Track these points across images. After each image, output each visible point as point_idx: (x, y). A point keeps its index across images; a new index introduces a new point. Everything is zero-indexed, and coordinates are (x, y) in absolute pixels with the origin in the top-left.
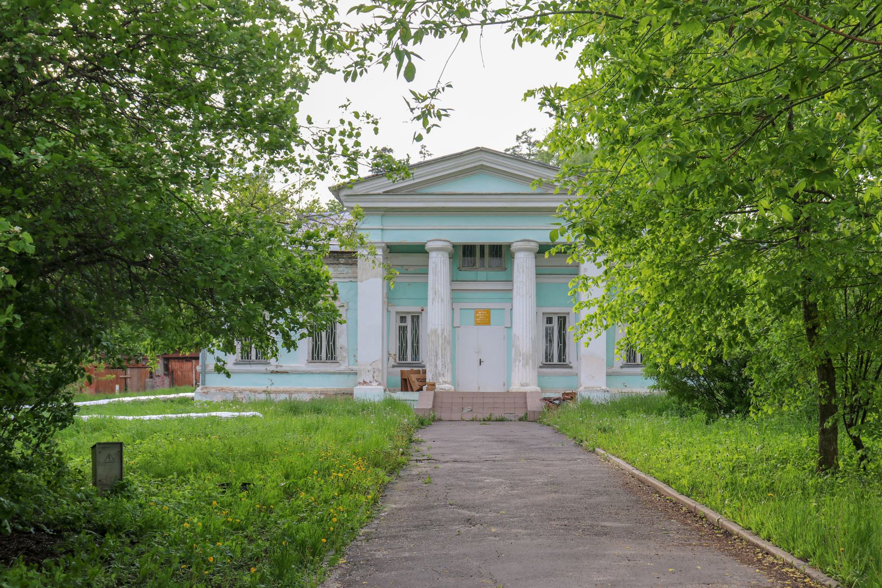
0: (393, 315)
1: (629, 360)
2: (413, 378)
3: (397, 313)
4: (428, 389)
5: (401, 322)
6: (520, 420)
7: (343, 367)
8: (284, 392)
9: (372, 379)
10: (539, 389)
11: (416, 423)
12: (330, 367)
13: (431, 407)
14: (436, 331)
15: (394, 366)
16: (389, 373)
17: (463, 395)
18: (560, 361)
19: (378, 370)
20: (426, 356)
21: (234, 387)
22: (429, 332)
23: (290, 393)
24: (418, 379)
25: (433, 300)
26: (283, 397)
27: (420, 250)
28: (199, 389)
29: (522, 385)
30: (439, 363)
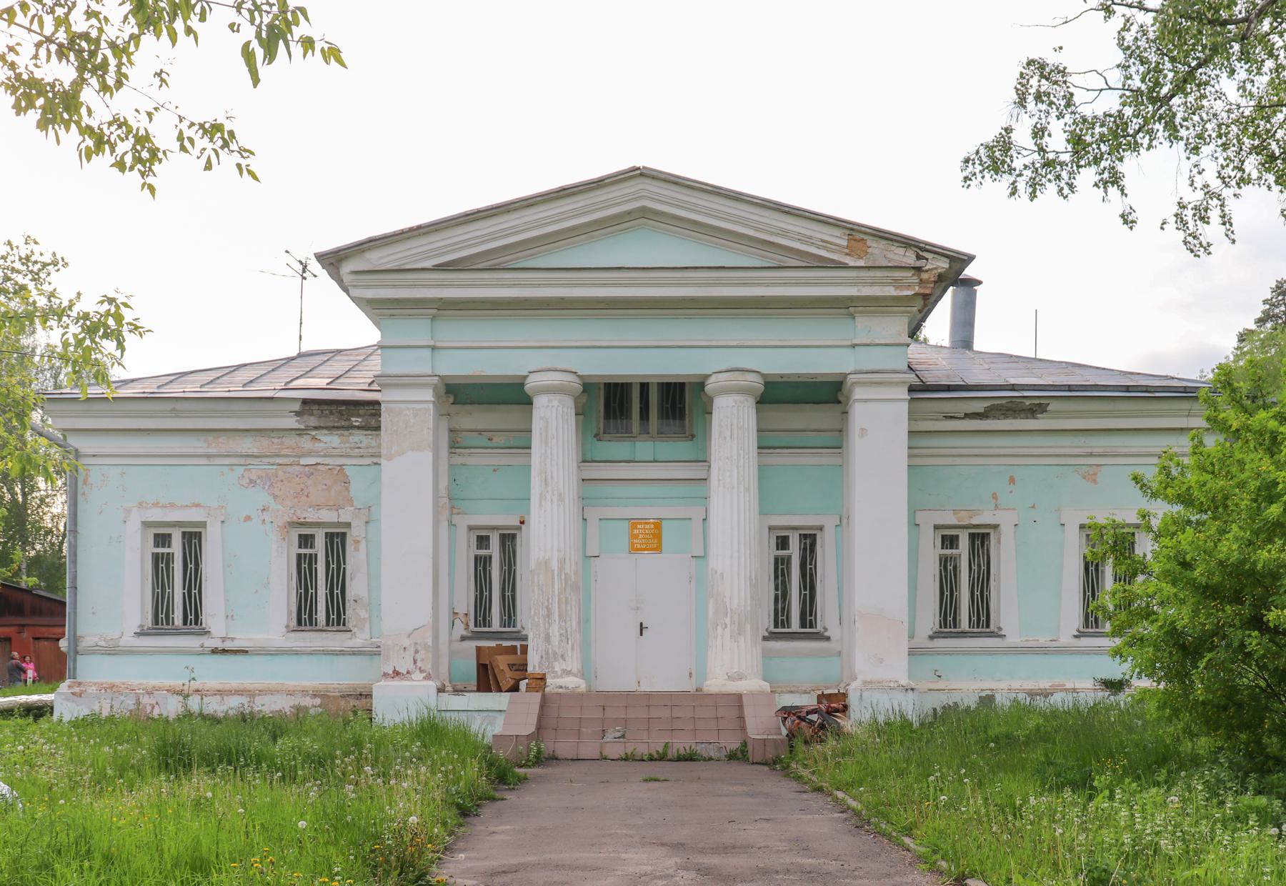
0: (462, 533)
1: (944, 623)
2: (502, 662)
3: (471, 528)
4: (529, 689)
5: (479, 547)
6: (732, 757)
7: (359, 639)
8: (239, 692)
9: (412, 667)
10: (766, 687)
11: (451, 817)
12: (333, 640)
13: (532, 729)
14: (547, 563)
15: (463, 638)
16: (452, 654)
17: (606, 700)
18: (803, 625)
19: (426, 647)
20: (527, 617)
21: (135, 682)
22: (533, 566)
23: (251, 694)
24: (511, 666)
25: (542, 497)
26: (233, 704)
27: (513, 395)
28: (64, 687)
29: (730, 678)
30: (555, 631)
